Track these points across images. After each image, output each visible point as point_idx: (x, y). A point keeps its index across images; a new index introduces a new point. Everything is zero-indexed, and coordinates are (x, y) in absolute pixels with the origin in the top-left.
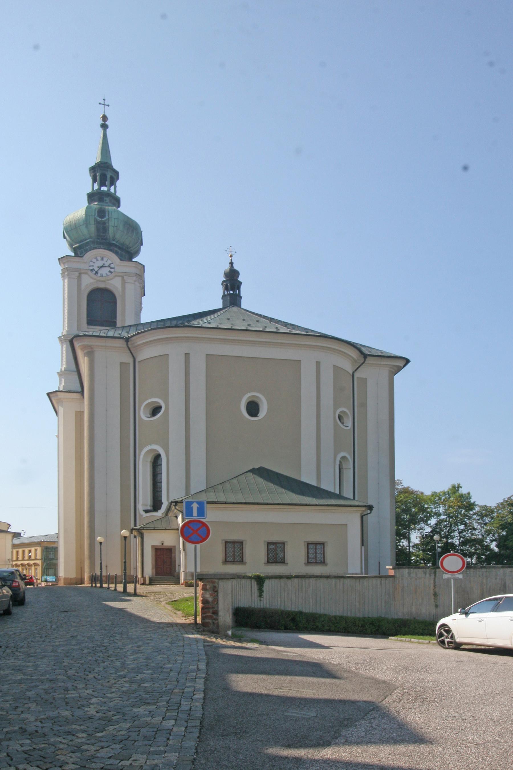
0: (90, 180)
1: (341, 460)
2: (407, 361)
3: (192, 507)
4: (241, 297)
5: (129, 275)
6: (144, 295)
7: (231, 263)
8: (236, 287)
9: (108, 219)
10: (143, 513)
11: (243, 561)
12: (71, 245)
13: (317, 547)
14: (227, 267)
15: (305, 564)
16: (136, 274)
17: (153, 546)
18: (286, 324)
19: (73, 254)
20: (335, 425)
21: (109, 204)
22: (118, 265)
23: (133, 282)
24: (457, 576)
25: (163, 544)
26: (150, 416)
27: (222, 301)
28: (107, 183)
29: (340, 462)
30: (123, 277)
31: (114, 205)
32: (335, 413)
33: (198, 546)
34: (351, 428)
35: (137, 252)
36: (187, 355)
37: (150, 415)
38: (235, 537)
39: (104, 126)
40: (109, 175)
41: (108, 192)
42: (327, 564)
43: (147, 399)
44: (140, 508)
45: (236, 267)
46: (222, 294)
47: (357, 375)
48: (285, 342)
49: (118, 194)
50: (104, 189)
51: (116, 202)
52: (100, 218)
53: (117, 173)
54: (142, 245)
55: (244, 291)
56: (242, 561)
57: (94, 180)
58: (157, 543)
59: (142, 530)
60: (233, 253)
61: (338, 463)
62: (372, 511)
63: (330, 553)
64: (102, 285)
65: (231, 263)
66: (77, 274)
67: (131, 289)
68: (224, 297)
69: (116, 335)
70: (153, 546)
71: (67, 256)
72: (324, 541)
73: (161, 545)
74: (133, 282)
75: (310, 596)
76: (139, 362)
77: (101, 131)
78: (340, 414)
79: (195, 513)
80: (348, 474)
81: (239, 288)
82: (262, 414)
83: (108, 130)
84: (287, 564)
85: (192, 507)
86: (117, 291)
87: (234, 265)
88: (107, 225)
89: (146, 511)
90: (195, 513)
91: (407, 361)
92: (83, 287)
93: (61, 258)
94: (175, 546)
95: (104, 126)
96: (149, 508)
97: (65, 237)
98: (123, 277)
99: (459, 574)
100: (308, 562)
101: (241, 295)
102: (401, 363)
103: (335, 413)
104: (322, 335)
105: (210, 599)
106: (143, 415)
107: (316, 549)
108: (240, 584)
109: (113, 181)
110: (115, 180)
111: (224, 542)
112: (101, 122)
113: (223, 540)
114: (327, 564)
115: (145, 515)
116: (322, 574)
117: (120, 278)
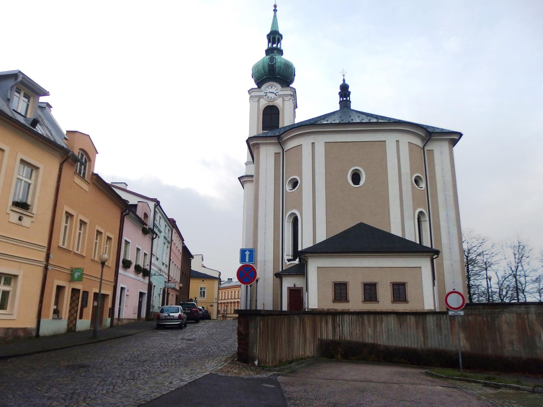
0: (267, 41)
1: (420, 215)
2: (460, 135)
3: (246, 254)
4: (351, 102)
5: (286, 95)
6: (297, 107)
7: (344, 80)
8: (347, 95)
9: (275, 63)
10: (286, 261)
11: (347, 300)
12: (255, 81)
13: (400, 288)
14: (342, 82)
15: (392, 302)
16: (291, 94)
17: (288, 288)
18: (367, 115)
19: (256, 87)
20: (413, 187)
21: (277, 54)
22: (280, 90)
23: (289, 100)
24: (459, 312)
25: (295, 286)
26: (291, 189)
27: (339, 105)
28: (276, 42)
29: (418, 216)
30: (283, 97)
31: (280, 54)
32: (411, 179)
33: (249, 285)
34: (425, 188)
35: (292, 81)
36: (313, 143)
37: (292, 188)
38: (341, 279)
39: (275, 11)
40: (277, 37)
41: (280, 49)
42: (408, 302)
43: (290, 177)
44: (286, 258)
45: (347, 82)
46: (339, 101)
47: (426, 148)
48: (368, 129)
49: (282, 48)
50: (275, 46)
51: (281, 52)
52: (271, 63)
53: (281, 36)
54: (295, 76)
55: (352, 98)
56: (346, 300)
57: (269, 42)
58: (291, 285)
59: (281, 275)
60: (345, 74)
61: (416, 217)
62: (439, 255)
63: (410, 291)
64: (271, 104)
65: (344, 80)
66: (258, 99)
67: (289, 104)
68: (340, 102)
69: (273, 135)
70: (288, 288)
71: (252, 88)
72: (405, 282)
73: (293, 286)
74: (289, 100)
75: (384, 330)
76: (285, 151)
77: (273, 13)
78: (416, 178)
79: (247, 260)
80: (426, 226)
81: (349, 96)
82: (362, 182)
83: (277, 12)
84: (379, 302)
85: (246, 254)
86: (280, 107)
87: (346, 81)
88: (275, 66)
89: (289, 260)
90: (247, 260)
91: (460, 135)
92: (261, 107)
93: (250, 90)
94: (302, 288)
95: (275, 11)
96: (291, 258)
97: (253, 77)
98: (283, 97)
99: (461, 310)
100: (335, 299)
101: (351, 100)
102: (456, 137)
103: (411, 179)
104: (396, 121)
105: (243, 332)
106: (288, 188)
107: (399, 289)
108: (309, 319)
109: (279, 41)
110: (281, 39)
111: (334, 283)
112: (273, 8)
113: (333, 282)
114: (408, 302)
115: (288, 263)
116: (405, 310)
117: (282, 98)
